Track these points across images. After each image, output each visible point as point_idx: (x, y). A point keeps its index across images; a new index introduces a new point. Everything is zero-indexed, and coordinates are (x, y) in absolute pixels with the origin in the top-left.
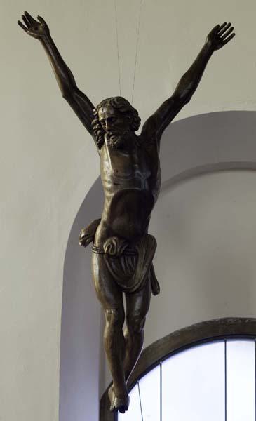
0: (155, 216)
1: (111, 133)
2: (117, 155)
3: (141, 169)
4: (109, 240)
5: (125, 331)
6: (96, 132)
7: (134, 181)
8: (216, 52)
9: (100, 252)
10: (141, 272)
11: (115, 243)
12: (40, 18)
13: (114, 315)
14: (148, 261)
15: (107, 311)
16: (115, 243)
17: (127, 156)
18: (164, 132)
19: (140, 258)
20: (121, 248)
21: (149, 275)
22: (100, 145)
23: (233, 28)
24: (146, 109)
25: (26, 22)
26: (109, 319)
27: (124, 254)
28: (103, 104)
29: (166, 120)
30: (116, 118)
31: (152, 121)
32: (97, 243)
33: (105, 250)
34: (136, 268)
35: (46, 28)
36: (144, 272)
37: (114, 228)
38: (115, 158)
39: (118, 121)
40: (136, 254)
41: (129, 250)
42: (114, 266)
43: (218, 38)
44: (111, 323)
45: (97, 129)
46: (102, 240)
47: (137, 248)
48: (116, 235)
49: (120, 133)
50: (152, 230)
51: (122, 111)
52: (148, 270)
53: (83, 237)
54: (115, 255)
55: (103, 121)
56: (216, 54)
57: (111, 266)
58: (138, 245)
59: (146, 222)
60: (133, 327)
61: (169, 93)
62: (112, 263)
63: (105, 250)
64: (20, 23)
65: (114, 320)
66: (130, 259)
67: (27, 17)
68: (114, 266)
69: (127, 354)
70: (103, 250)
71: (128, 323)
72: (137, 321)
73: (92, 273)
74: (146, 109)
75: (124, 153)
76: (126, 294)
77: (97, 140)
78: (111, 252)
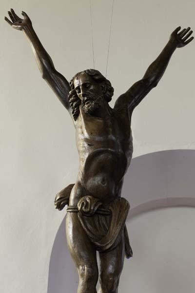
0: (127, 178)
1: (86, 98)
2: (91, 121)
3: (114, 133)
4: (82, 199)
5: (62, 203)
6: (72, 105)
7: (108, 143)
8: (178, 50)
9: (75, 210)
10: (115, 231)
11: (88, 201)
12: (24, 14)
13: (88, 271)
14: (121, 222)
15: (81, 268)
16: (88, 201)
17: (101, 121)
18: (135, 109)
19: (113, 218)
20: (95, 206)
21: (123, 235)
22: (76, 116)
23: (192, 32)
24: (120, 87)
25: (11, 17)
26: (82, 275)
27: (97, 213)
28: (78, 76)
29: (136, 97)
30: (91, 84)
31: (123, 98)
32: (71, 203)
33: (79, 208)
34: (109, 227)
35: (29, 21)
36: (118, 231)
37: (88, 188)
38: (90, 123)
39: (92, 88)
40: (111, 214)
41: (103, 209)
42: (89, 226)
43: (178, 39)
44: (85, 279)
45: (73, 101)
46: (77, 198)
47: (110, 208)
48: (90, 195)
49: (94, 98)
50: (124, 193)
51: (96, 82)
52: (121, 231)
53: (58, 200)
54: (88, 212)
55: (78, 88)
56: (178, 51)
57: (87, 227)
58: (112, 206)
59: (119, 184)
60: (107, 285)
61: (140, 76)
62: (86, 221)
63: (79, 208)
64: (6, 19)
65: (88, 276)
66: (106, 218)
67: (12, 14)
68: (89, 226)
69: (61, 80)
70: (77, 209)
71: (103, 282)
72: (111, 279)
73: (103, 288)
74: (120, 87)
75: (99, 119)
76: (100, 253)
77: (73, 113)
78: (85, 208)
